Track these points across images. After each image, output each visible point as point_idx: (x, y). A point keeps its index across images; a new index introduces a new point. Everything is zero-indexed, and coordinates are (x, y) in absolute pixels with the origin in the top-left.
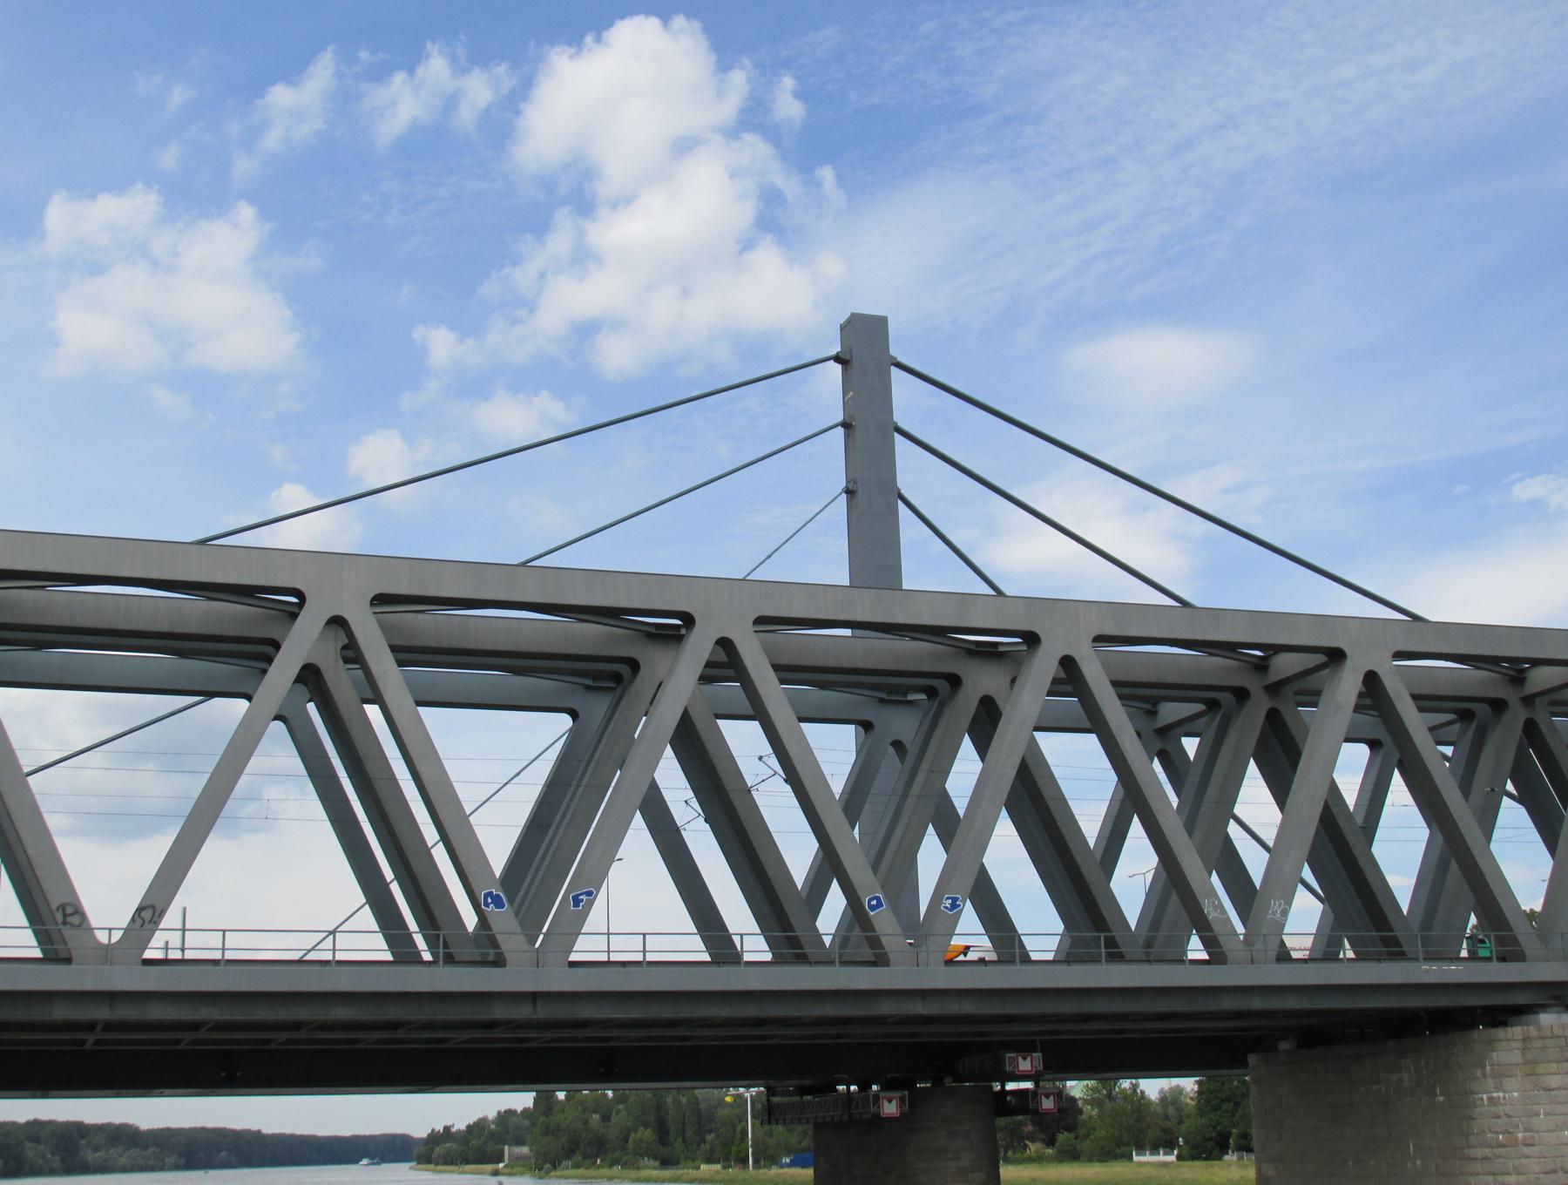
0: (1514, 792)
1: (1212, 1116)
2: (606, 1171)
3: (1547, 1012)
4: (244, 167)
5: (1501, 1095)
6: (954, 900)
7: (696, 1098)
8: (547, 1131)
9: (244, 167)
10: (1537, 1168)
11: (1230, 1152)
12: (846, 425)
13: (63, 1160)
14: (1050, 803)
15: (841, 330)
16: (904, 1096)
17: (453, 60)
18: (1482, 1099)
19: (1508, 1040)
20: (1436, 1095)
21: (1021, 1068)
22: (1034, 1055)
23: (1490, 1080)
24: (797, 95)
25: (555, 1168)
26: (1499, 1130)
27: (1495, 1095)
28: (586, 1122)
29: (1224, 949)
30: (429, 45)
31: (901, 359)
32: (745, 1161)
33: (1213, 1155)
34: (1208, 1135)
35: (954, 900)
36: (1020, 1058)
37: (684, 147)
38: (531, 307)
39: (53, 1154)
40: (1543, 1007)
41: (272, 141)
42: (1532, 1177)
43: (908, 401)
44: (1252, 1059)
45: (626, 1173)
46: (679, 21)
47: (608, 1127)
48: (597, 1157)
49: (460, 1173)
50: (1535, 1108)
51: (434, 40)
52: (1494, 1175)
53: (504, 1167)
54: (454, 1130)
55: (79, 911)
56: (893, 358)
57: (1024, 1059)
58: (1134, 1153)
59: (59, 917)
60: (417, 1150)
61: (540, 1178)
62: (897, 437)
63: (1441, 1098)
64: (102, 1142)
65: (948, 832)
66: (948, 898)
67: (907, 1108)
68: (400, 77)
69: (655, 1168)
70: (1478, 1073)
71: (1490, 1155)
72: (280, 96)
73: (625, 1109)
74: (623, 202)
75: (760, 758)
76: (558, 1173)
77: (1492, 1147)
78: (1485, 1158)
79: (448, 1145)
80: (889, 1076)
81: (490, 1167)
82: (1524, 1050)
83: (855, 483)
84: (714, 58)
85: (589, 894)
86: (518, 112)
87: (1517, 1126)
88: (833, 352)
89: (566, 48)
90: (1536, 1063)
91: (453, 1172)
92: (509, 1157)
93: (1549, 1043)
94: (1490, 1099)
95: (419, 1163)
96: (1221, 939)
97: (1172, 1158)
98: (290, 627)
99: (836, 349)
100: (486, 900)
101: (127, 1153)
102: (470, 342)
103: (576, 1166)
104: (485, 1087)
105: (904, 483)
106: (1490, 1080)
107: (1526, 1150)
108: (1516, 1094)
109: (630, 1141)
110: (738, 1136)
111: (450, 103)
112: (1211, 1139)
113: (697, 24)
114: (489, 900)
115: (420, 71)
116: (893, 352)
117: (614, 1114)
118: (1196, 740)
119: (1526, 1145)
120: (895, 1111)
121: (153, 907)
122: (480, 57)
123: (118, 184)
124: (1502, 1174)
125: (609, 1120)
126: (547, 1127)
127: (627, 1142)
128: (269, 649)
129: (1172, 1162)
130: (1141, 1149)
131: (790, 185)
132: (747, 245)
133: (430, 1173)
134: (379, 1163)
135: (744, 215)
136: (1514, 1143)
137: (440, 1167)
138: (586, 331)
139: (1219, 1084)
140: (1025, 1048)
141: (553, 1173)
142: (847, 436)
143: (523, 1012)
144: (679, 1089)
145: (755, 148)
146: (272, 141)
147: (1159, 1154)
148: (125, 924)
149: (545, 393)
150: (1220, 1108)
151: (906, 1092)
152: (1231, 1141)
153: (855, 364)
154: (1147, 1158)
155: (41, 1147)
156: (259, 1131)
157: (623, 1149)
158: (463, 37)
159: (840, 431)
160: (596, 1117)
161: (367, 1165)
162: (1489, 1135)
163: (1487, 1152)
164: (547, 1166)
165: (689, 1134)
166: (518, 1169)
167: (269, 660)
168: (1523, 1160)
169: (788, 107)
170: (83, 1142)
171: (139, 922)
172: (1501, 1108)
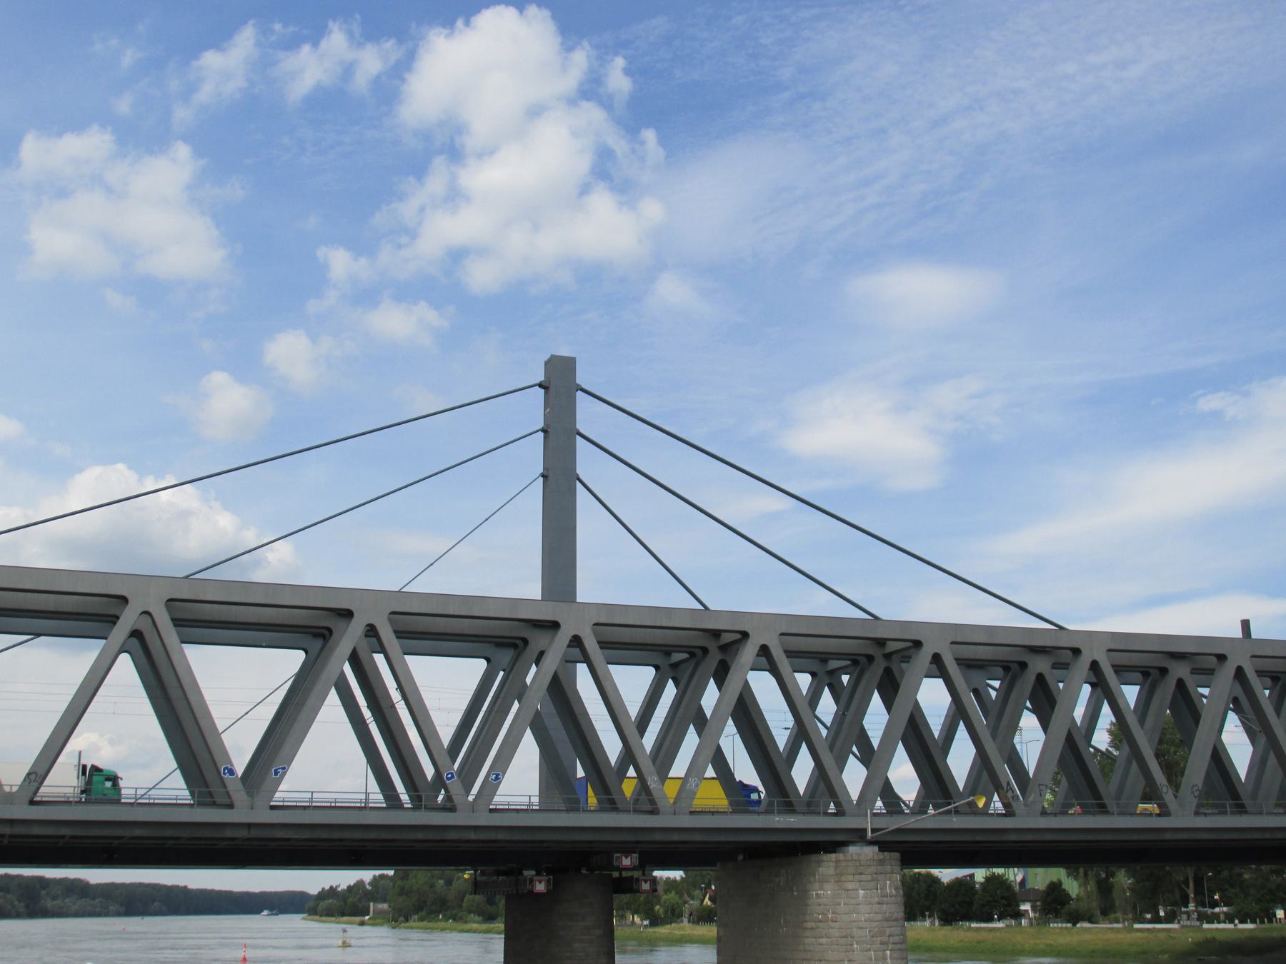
0: (990, 689)
2: (442, 924)
3: (854, 846)
4: (182, 115)
5: (822, 892)
6: (497, 775)
8: (402, 891)
9: (182, 115)
10: (837, 934)
12: (544, 431)
13: (27, 907)
14: (579, 717)
15: (545, 365)
16: (550, 879)
17: (350, 34)
18: (813, 895)
19: (828, 861)
20: (793, 891)
21: (624, 863)
22: (634, 855)
23: (817, 884)
24: (627, 72)
25: (407, 920)
26: (819, 912)
27: (819, 892)
28: (432, 886)
29: (659, 806)
30: (331, 24)
31: (584, 386)
35: (497, 775)
36: (623, 857)
37: (535, 112)
38: (413, 234)
39: (20, 902)
40: (853, 843)
41: (205, 94)
42: (834, 939)
43: (587, 415)
44: (718, 864)
45: (455, 925)
46: (532, 10)
47: (450, 889)
48: (439, 913)
49: (337, 923)
50: (839, 900)
51: (335, 20)
52: (816, 938)
53: (369, 919)
54: (339, 889)
56: (578, 385)
57: (626, 857)
60: (311, 904)
61: (394, 928)
63: (796, 893)
64: (59, 893)
66: (493, 774)
68: (306, 49)
69: (479, 922)
70: (812, 879)
71: (814, 926)
72: (211, 59)
74: (487, 153)
76: (407, 924)
77: (816, 922)
78: (812, 928)
79: (330, 901)
81: (358, 919)
82: (836, 868)
83: (548, 470)
84: (559, 39)
85: (284, 768)
86: (403, 80)
87: (829, 911)
88: (538, 382)
89: (441, 30)
91: (331, 922)
93: (850, 863)
94: (816, 894)
95: (310, 915)
96: (657, 800)
98: (125, 608)
99: (541, 378)
100: (224, 771)
101: (79, 902)
102: (363, 261)
103: (421, 919)
104: (1227, 765)
106: (817, 884)
107: (832, 924)
108: (829, 892)
109: (465, 900)
111: (348, 70)
113: (546, 13)
114: (226, 771)
115: (324, 44)
116: (578, 381)
117: (455, 880)
119: (832, 921)
122: (371, 33)
123: (78, 125)
124: (820, 938)
125: (451, 884)
127: (462, 901)
128: (114, 619)
131: (619, 145)
132: (585, 190)
133: (316, 923)
134: (277, 914)
135: (583, 164)
136: (826, 920)
137: (323, 918)
138: (458, 255)
141: (403, 925)
142: (545, 438)
143: (243, 833)
144: (417, 870)
145: (593, 114)
146: (205, 94)
148: (19, 783)
149: (423, 303)
151: (551, 877)
153: (552, 390)
155: (9, 896)
156: (185, 887)
157: (460, 906)
158: (357, 16)
159: (541, 434)
160: (441, 882)
161: (268, 915)
162: (815, 915)
163: (813, 924)
164: (402, 919)
166: (378, 921)
167: (115, 623)
168: (830, 930)
169: (618, 80)
170: (44, 892)
171: (28, 781)
172: (821, 900)
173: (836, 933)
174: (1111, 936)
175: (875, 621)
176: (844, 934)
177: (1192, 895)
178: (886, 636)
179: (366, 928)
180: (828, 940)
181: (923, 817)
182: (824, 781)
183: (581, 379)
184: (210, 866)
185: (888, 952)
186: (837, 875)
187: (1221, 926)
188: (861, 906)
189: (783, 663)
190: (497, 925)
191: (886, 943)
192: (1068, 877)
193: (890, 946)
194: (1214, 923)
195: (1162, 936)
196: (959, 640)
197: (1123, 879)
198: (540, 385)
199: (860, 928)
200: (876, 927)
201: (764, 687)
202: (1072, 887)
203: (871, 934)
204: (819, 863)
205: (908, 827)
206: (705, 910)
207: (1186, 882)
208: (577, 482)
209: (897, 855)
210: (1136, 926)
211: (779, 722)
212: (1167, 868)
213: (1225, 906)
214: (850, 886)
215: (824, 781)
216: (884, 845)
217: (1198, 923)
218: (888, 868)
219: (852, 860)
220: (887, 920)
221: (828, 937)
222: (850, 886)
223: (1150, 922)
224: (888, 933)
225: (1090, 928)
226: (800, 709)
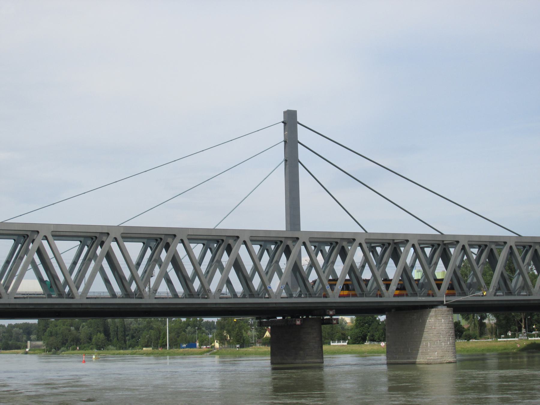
0: (473, 254)
1: (361, 329)
7: (115, 322)
10: (435, 333)
11: (367, 342)
31: (300, 122)
32: (164, 346)
33: (361, 343)
34: (359, 336)
43: (302, 135)
55: (210, 290)
57: (331, 311)
58: (331, 342)
59: (207, 291)
62: (299, 144)
63: (421, 321)
65: (222, 269)
67: (302, 323)
73: (87, 325)
75: (306, 260)
76: (68, 352)
78: (427, 331)
80: (297, 315)
90: (437, 315)
92: (30, 346)
97: (345, 344)
105: (300, 158)
110: (162, 336)
112: (360, 337)
117: (81, 327)
118: (329, 247)
120: (299, 323)
121: (220, 290)
126: (51, 332)
129: (346, 345)
130: (334, 341)
136: (432, 329)
139: (364, 317)
140: (331, 310)
147: (336, 343)
150: (364, 326)
152: (367, 338)
154: (336, 344)
162: (428, 327)
165: (120, 336)
173: (435, 332)
174: (488, 343)
175: (442, 235)
176: (438, 333)
177: (523, 326)
178: (444, 240)
179: (28, 355)
180: (433, 335)
181: (465, 297)
182: (264, 285)
183: (299, 120)
184: (31, 318)
185: (451, 338)
186: (435, 315)
187: (536, 339)
188: (443, 324)
189: (249, 243)
190: (137, 350)
191: (450, 335)
192: (463, 319)
193: (451, 336)
194: (533, 337)
195: (513, 343)
196: (470, 240)
197: (490, 320)
198: (283, 122)
199: (443, 331)
200: (447, 330)
201: (243, 252)
202: (464, 324)
203: (446, 332)
204: (430, 312)
205: (461, 300)
206: (268, 339)
207: (521, 321)
208: (299, 163)
209: (452, 309)
210: (499, 340)
211: (248, 265)
212: (513, 314)
213: (537, 331)
214: (439, 318)
215: (264, 285)
216: (448, 306)
217: (527, 338)
218: (451, 313)
219: (440, 310)
220: (450, 328)
221: (432, 334)
222: (439, 318)
223: (503, 338)
224: (450, 332)
225: (478, 341)
226: (256, 260)
